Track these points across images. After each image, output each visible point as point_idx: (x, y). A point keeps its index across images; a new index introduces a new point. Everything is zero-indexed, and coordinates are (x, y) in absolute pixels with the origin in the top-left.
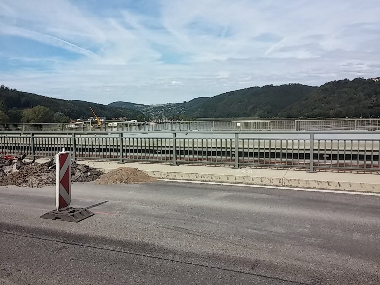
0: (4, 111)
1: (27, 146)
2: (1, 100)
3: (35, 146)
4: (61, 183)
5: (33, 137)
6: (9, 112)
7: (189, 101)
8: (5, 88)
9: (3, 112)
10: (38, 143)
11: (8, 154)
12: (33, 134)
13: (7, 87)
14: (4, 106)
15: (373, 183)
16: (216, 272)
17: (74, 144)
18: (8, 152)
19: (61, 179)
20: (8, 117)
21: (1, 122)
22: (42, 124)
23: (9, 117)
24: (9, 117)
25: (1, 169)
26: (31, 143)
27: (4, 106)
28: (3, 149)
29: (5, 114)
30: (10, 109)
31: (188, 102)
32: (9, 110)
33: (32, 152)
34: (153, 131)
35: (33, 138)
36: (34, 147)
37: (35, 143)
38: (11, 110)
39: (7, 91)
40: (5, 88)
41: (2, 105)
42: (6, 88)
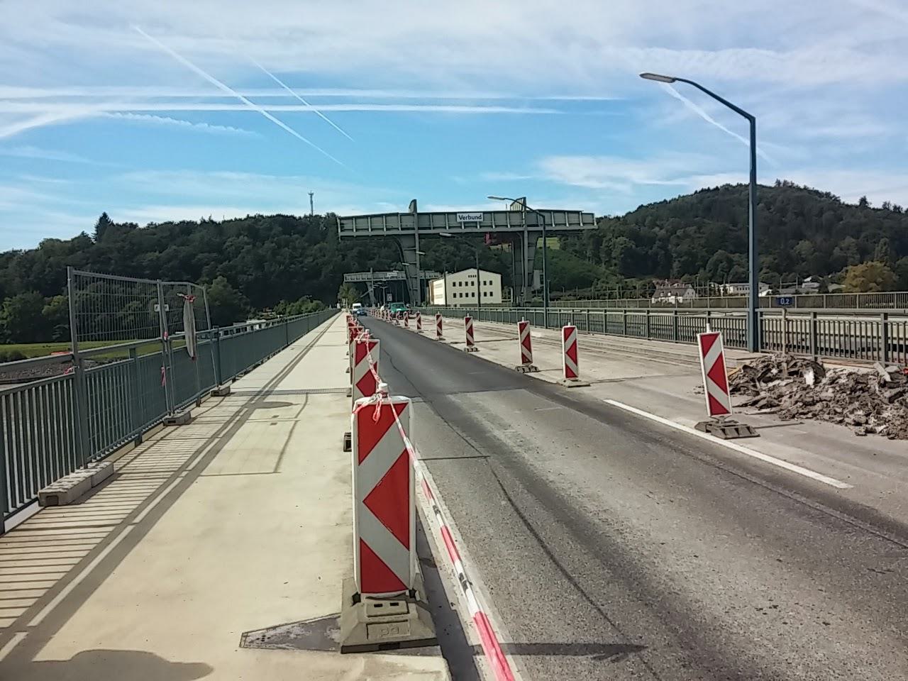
0: (887, 262)
1: (899, 342)
2: (883, 238)
3: (890, 342)
4: (569, 355)
5: (886, 321)
6: (899, 265)
7: (636, 209)
8: (892, 208)
9: (885, 265)
10: (895, 335)
11: (867, 359)
12: (886, 316)
13: (898, 206)
14: (889, 252)
15: (673, 394)
16: (84, 292)
17: (883, 335)
18: (873, 357)
19: (569, 347)
20: (895, 278)
21: (880, 289)
22: (895, 293)
23: (899, 275)
24: (898, 277)
25: (903, 399)
26: (880, 335)
27: (889, 252)
28: (894, 353)
29: (889, 268)
30: (901, 256)
31: (636, 211)
32: (898, 260)
33: (882, 354)
34: (751, 288)
35: (886, 325)
36: (887, 347)
37: (889, 335)
38: (903, 259)
39: (896, 215)
40: (892, 208)
41: (884, 248)
42: (895, 207)
